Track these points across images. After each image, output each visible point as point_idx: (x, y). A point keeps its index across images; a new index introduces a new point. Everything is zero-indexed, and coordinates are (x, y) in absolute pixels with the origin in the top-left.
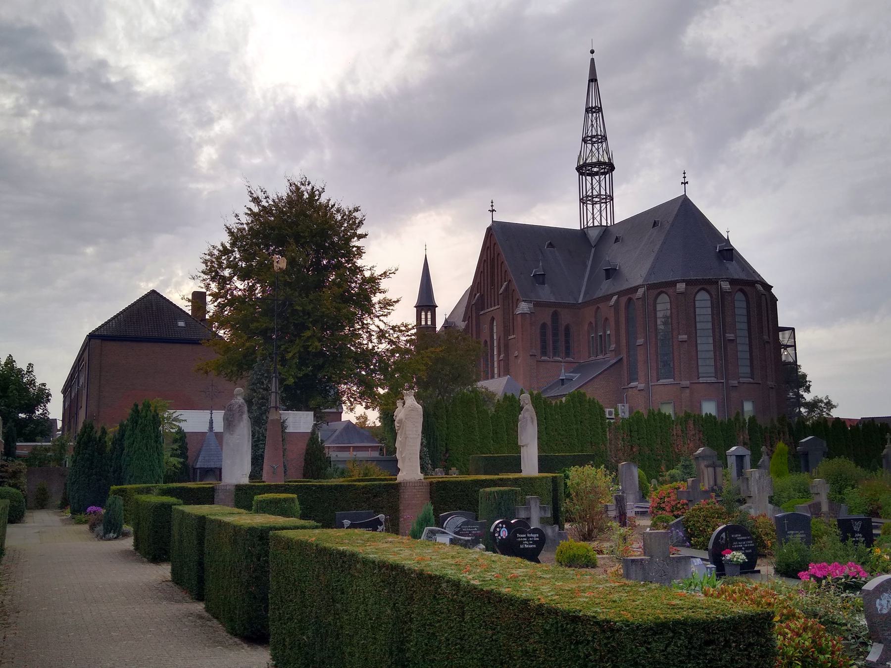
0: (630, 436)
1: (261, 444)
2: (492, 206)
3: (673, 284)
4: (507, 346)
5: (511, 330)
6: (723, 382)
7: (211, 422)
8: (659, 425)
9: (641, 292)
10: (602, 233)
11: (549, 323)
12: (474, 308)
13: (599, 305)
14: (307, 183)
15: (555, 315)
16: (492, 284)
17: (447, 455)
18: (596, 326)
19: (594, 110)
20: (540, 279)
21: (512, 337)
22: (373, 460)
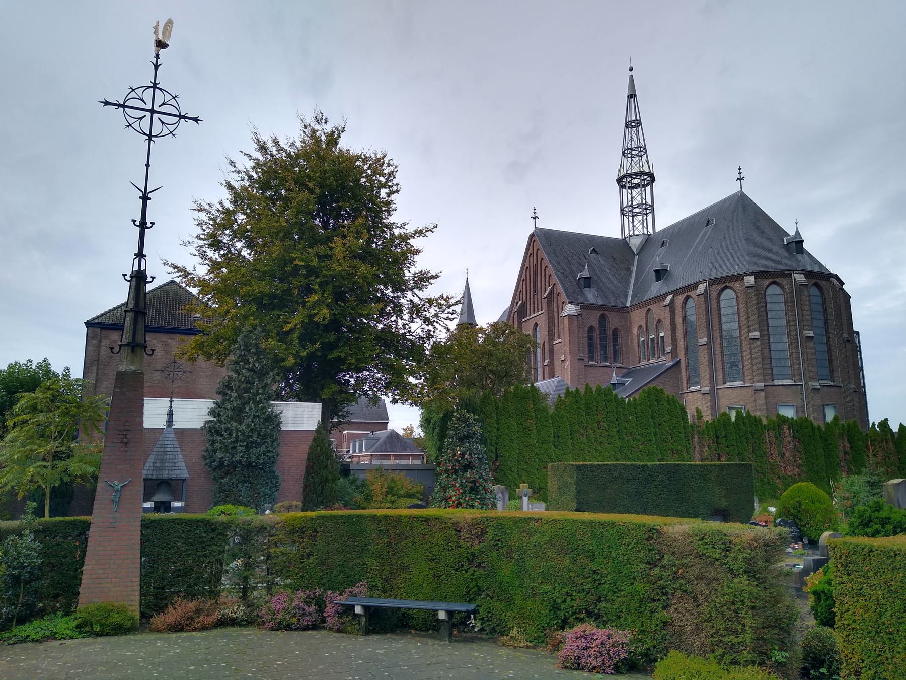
0: (717, 443)
1: (240, 446)
2: (535, 213)
3: (740, 277)
4: (551, 352)
5: (556, 335)
6: (802, 385)
7: (170, 414)
8: (749, 429)
9: (701, 288)
10: (644, 242)
11: (597, 326)
12: (516, 316)
13: (650, 307)
14: (323, 121)
15: (603, 318)
16: (535, 290)
17: (498, 464)
18: (647, 330)
19: (634, 124)
20: (587, 282)
21: (558, 341)
22: (409, 470)
